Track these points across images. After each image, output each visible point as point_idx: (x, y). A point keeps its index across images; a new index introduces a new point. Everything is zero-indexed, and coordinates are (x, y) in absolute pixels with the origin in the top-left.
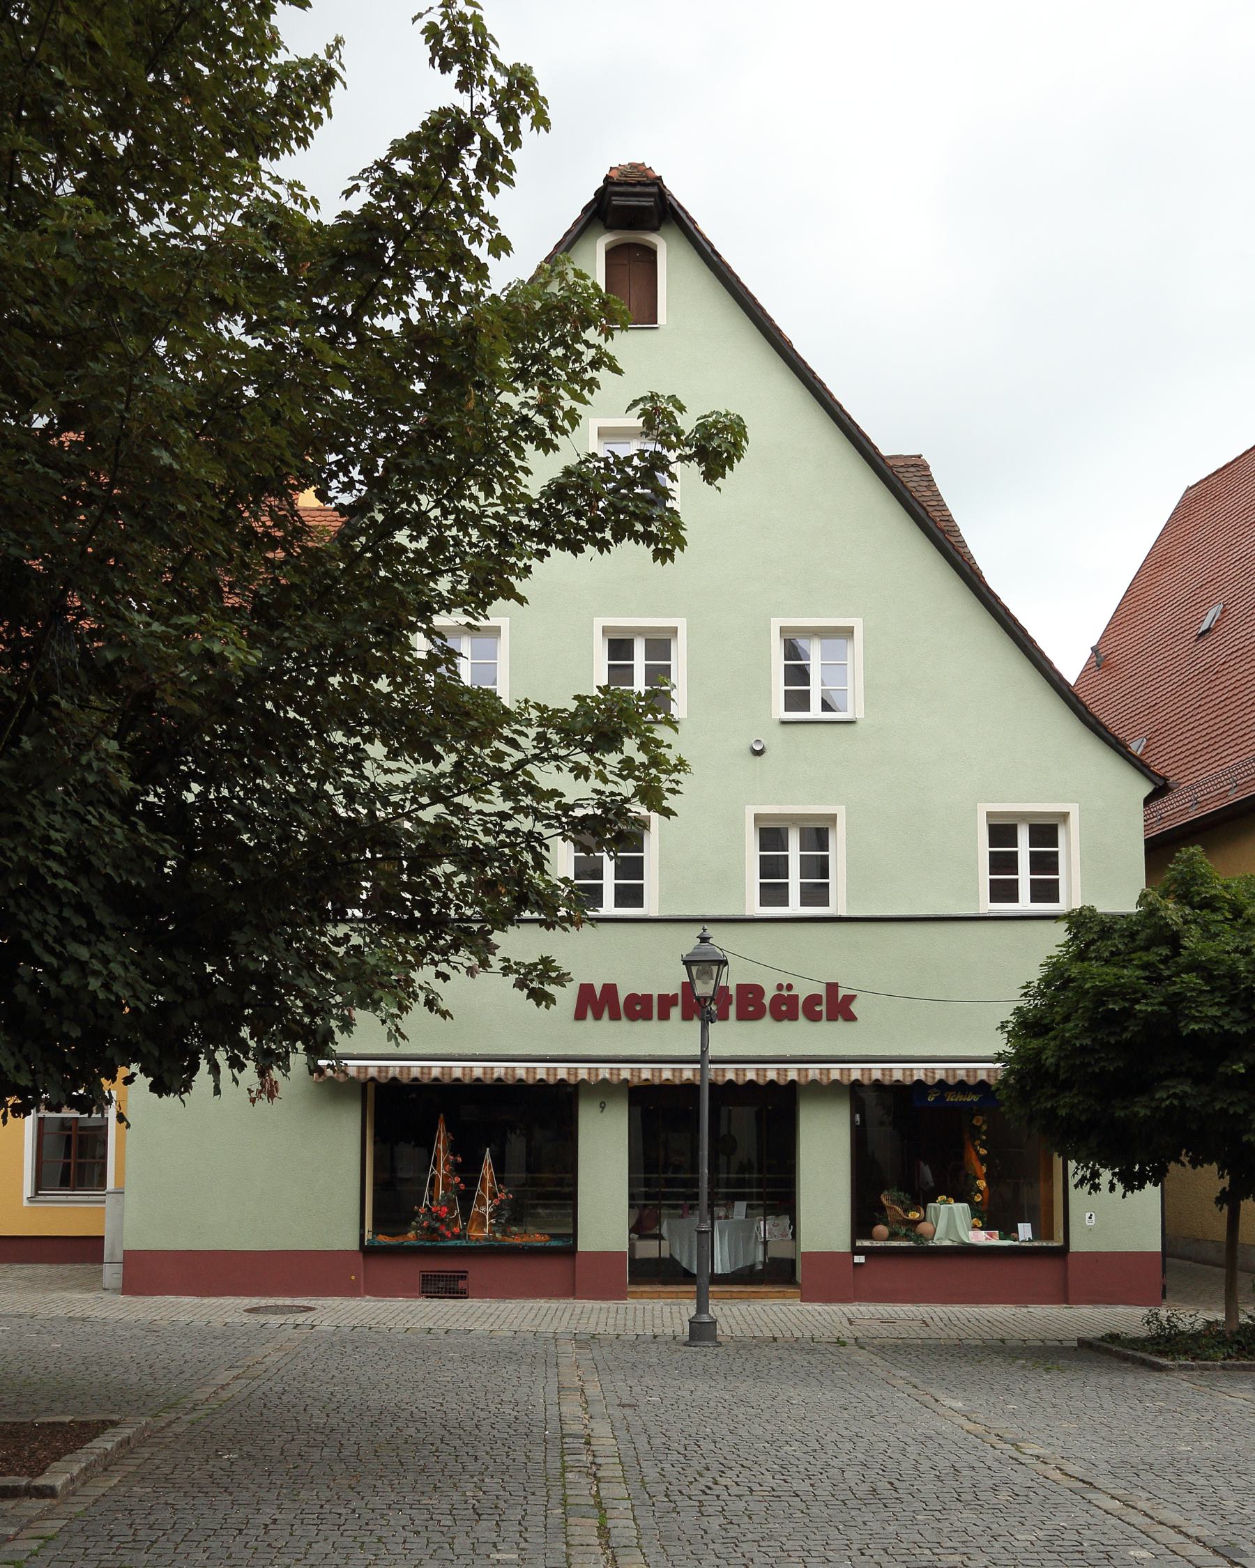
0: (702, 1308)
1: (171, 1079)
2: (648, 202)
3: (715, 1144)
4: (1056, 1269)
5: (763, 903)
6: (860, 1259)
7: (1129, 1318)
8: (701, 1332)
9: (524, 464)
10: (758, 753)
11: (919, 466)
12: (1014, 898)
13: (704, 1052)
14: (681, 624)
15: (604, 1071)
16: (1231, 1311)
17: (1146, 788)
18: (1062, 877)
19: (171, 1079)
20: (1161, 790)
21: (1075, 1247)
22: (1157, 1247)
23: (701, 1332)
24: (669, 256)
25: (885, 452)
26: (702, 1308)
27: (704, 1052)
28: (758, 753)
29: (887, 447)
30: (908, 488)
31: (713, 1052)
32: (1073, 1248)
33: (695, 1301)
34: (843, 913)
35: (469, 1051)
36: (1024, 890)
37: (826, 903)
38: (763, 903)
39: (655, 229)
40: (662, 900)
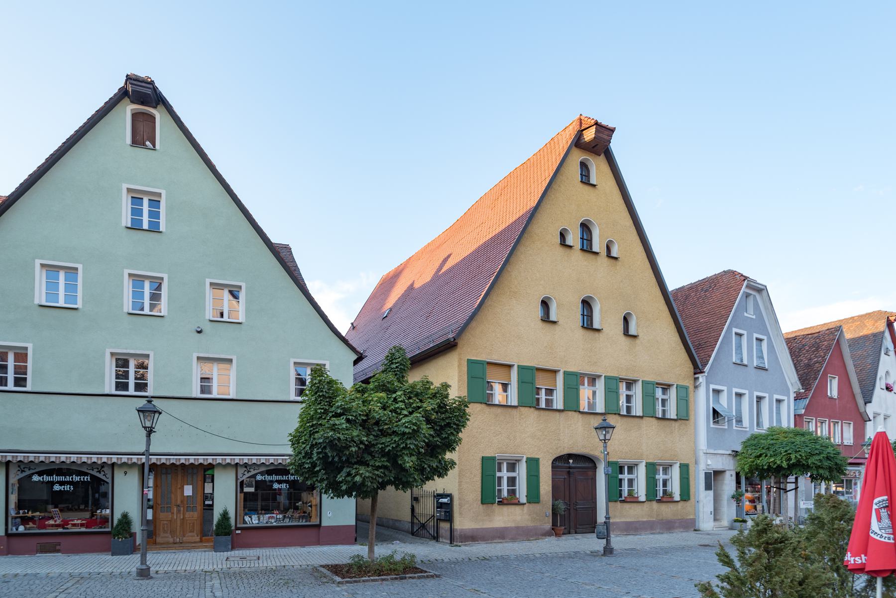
0: (143, 561)
4: (316, 533)
5: (116, 390)
6: (239, 532)
7: (343, 553)
10: (199, 332)
11: (287, 248)
12: (127, 389)
17: (355, 357)
18: (114, 380)
20: (360, 359)
22: (353, 522)
23: (144, 573)
25: (273, 241)
26: (143, 561)
28: (199, 332)
29: (274, 239)
30: (282, 256)
31: (152, 450)
33: (530, 524)
36: (132, 386)
37: (25, 386)
38: (116, 390)
40: (33, 384)
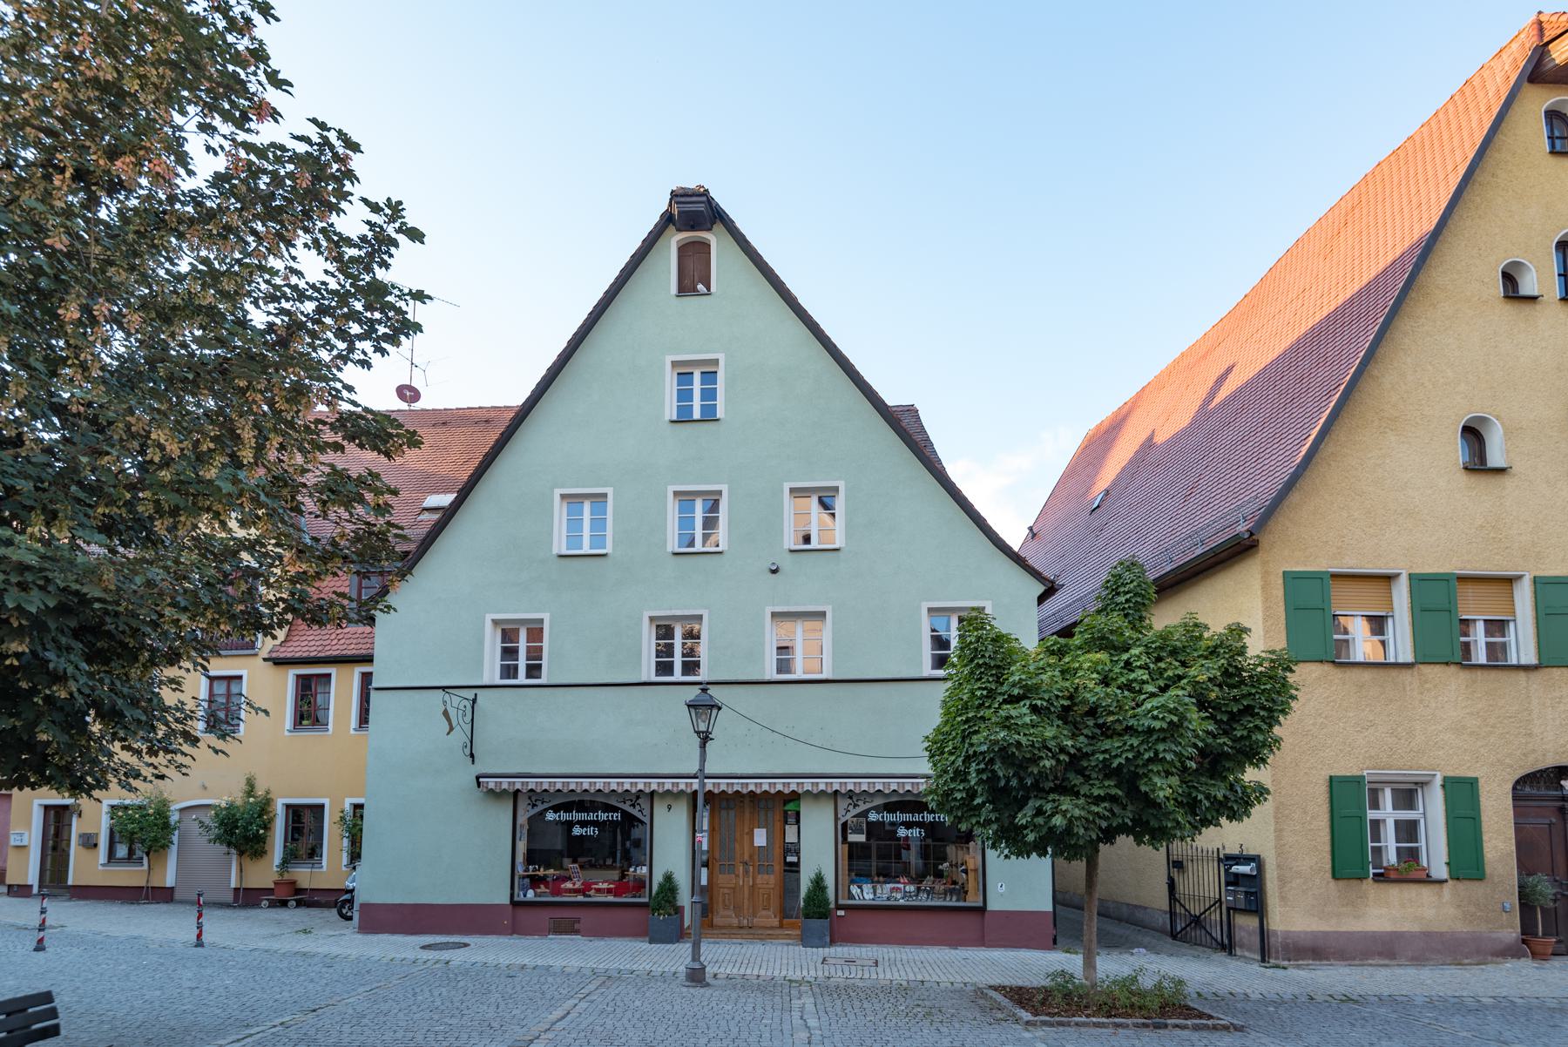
0: (696, 956)
1: (21, 789)
2: (701, 207)
3: (579, 851)
4: (976, 923)
6: (841, 913)
8: (696, 976)
9: (375, 218)
10: (774, 572)
11: (911, 411)
13: (701, 770)
14: (724, 488)
15: (668, 784)
16: (1089, 964)
19: (21, 789)
20: (1050, 590)
21: (993, 906)
23: (696, 976)
24: (715, 239)
25: (890, 402)
27: (701, 770)
28: (774, 572)
29: (891, 400)
30: (905, 426)
31: (709, 770)
32: (989, 908)
34: (830, 677)
35: (649, 771)
39: (709, 229)
